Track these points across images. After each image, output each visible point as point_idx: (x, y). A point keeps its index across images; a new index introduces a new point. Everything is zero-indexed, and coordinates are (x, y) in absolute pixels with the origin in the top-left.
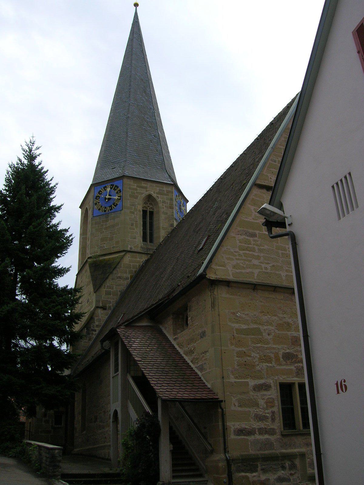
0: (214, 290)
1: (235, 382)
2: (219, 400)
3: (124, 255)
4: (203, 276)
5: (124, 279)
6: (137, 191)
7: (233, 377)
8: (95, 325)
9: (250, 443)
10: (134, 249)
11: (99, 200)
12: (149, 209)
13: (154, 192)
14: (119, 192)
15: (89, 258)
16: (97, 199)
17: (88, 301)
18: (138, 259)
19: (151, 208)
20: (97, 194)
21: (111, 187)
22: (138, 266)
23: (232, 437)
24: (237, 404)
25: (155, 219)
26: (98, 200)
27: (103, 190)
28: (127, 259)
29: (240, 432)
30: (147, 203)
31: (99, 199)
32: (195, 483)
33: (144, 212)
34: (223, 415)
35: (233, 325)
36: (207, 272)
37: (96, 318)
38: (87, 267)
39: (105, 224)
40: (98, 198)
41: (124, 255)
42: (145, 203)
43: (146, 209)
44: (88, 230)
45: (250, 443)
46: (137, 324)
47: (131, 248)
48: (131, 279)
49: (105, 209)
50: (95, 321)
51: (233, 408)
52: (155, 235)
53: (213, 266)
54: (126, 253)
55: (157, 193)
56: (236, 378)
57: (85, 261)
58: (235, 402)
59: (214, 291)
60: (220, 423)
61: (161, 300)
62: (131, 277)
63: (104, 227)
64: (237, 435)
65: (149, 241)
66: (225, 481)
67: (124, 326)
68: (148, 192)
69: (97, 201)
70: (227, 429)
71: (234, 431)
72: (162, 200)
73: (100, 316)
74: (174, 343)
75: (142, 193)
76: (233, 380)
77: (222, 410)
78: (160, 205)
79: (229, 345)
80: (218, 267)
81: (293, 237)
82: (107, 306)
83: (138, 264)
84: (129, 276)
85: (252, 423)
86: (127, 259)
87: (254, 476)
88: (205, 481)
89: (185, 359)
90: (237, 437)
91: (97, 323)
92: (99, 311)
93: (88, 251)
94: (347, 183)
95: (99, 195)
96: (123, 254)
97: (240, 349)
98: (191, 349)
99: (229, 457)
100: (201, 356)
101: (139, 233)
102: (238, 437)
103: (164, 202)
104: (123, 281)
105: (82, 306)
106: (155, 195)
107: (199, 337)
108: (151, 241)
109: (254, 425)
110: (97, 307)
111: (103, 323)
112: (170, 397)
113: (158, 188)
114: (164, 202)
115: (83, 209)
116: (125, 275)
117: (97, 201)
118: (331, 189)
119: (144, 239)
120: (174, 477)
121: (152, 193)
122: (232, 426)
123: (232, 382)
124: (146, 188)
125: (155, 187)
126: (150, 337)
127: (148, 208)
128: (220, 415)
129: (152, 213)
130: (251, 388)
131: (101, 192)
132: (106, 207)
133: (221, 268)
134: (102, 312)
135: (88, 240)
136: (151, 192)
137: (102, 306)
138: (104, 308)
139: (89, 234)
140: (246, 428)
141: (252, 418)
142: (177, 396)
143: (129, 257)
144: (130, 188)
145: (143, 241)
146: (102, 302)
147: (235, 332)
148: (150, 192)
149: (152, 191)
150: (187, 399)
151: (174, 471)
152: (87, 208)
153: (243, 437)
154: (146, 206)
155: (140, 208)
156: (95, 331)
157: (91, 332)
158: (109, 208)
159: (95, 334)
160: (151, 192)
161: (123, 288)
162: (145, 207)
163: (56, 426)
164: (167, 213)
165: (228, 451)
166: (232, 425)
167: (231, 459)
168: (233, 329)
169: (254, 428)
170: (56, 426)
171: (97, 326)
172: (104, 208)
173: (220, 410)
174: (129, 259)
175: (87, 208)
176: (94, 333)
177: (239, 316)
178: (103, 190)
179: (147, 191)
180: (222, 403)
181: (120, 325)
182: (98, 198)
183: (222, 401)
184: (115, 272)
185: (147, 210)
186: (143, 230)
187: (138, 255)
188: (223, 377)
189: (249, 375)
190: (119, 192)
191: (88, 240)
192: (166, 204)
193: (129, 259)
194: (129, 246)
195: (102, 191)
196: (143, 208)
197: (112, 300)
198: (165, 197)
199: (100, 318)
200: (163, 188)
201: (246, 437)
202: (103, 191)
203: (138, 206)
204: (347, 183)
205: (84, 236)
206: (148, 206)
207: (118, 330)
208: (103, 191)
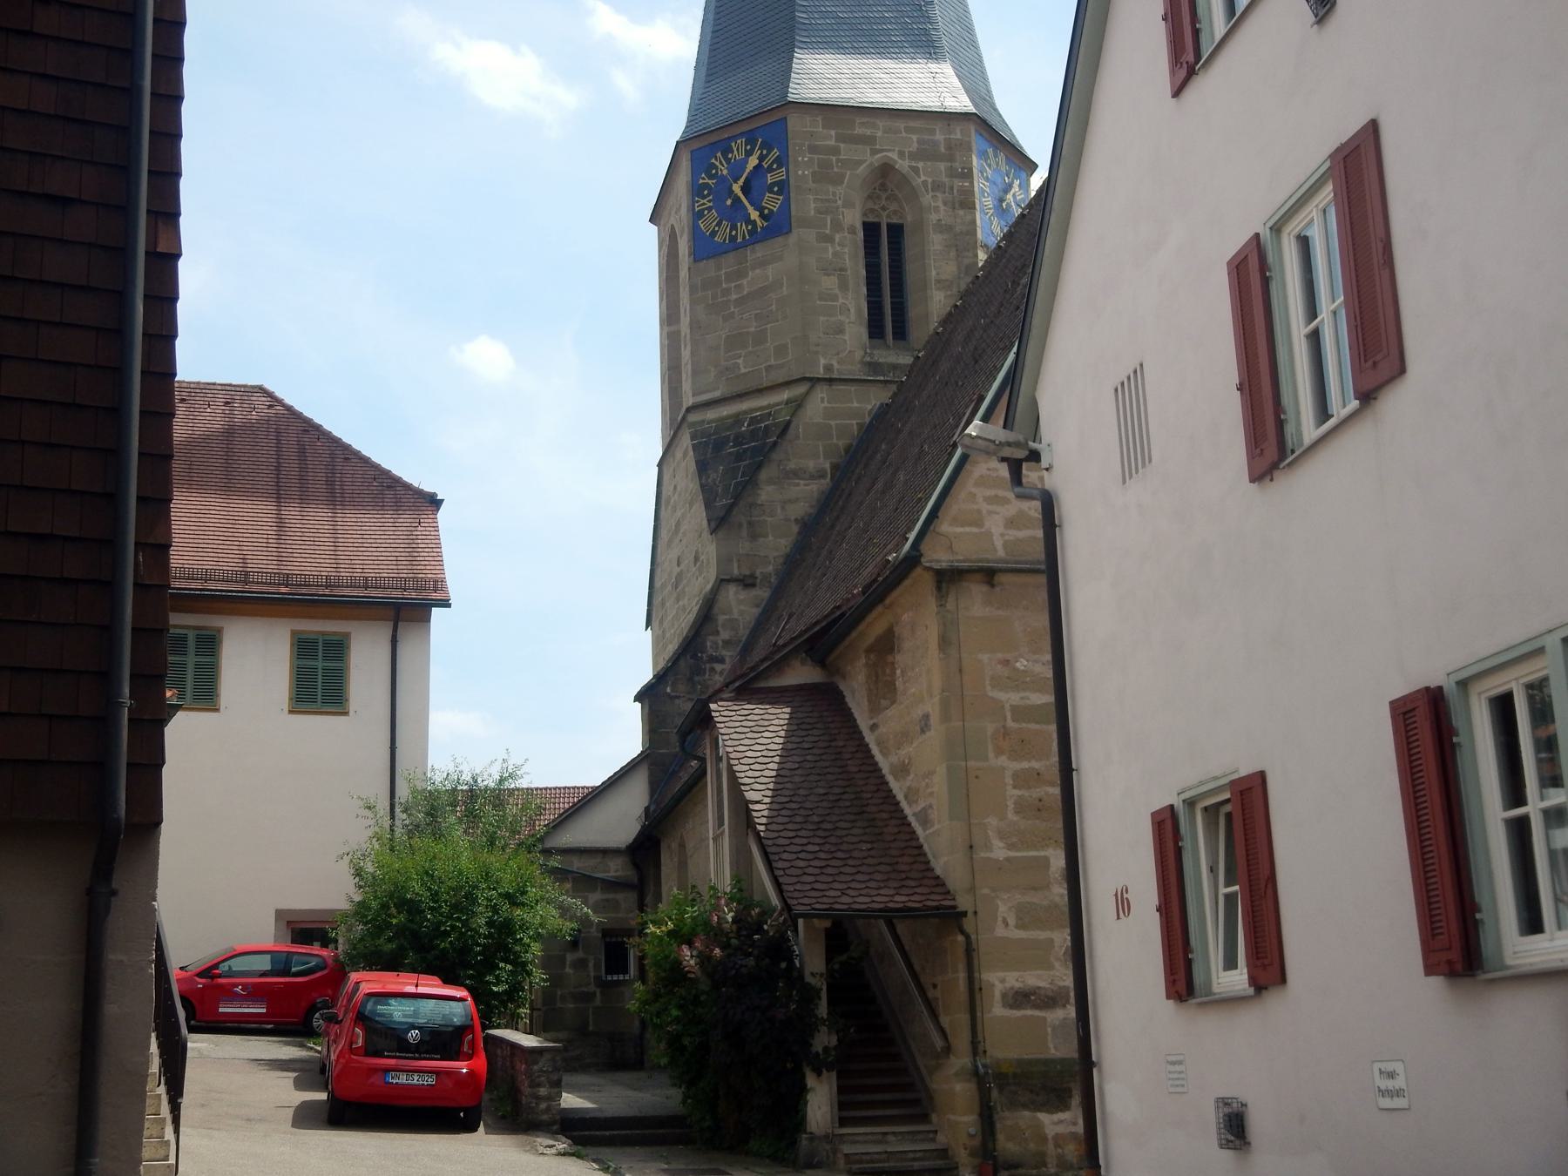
0: (947, 597)
1: (1008, 859)
2: (958, 910)
3: (808, 393)
4: (913, 560)
5: (812, 477)
6: (841, 157)
7: (1001, 845)
8: (720, 643)
9: (1049, 1030)
10: (839, 370)
11: (709, 201)
12: (888, 216)
13: (901, 154)
14: (775, 166)
15: (689, 410)
16: (704, 197)
17: (696, 559)
18: (855, 405)
19: (895, 212)
20: (703, 179)
21: (749, 147)
22: (855, 427)
23: (997, 1010)
24: (1012, 921)
25: (910, 251)
26: (705, 201)
27: (721, 162)
28: (818, 404)
29: (1021, 998)
30: (879, 197)
31: (708, 195)
32: (900, 1138)
33: (871, 230)
34: (970, 951)
35: (1001, 696)
36: (924, 548)
37: (721, 618)
38: (686, 441)
39: (735, 286)
40: (706, 192)
41: (808, 393)
42: (870, 197)
43: (876, 220)
44: (682, 311)
45: (1049, 1030)
46: (763, 684)
47: (828, 368)
48: (832, 478)
49: (731, 232)
50: (720, 629)
51: (1000, 931)
52: (913, 312)
53: (945, 526)
54: (812, 387)
55: (913, 156)
56: (1011, 847)
57: (679, 418)
58: (1005, 915)
59: (946, 601)
60: (962, 975)
61: (838, 608)
62: (835, 467)
63: (734, 297)
64: (1011, 1007)
65: (894, 333)
66: (973, 1133)
67: (731, 692)
68: (879, 155)
69: (704, 204)
70: (981, 989)
71: (1004, 996)
72: (930, 180)
73: (735, 611)
74: (870, 738)
75: (860, 163)
76: (999, 852)
77: (968, 937)
78: (926, 199)
79: (991, 755)
80: (959, 530)
81: (1048, 504)
82: (758, 574)
83: (854, 422)
84: (827, 466)
85: (1057, 974)
86: (818, 404)
87: (1061, 1122)
88: (929, 1132)
89: (891, 791)
90: (1011, 1011)
91: (725, 635)
92: (732, 594)
93: (687, 386)
94: (1136, 381)
95: (707, 181)
96: (800, 390)
97: (1025, 765)
98: (904, 761)
99: (984, 1066)
100: (924, 784)
101: (852, 310)
102: (1014, 1011)
103: (937, 187)
104: (805, 485)
105: (681, 571)
106: (903, 165)
107: (918, 728)
108: (901, 333)
109: (1065, 978)
110: (721, 582)
111: (744, 633)
112: (817, 906)
113: (915, 138)
114: (937, 187)
115: (661, 228)
116: (811, 465)
117: (704, 204)
118: (1113, 391)
119: (875, 329)
120: (843, 1122)
121: (894, 156)
122: (997, 983)
123: (997, 861)
124: (869, 140)
125: (904, 134)
126: (803, 723)
127: (884, 214)
128: (961, 952)
129: (896, 231)
130: (1057, 875)
131: (716, 168)
132: (736, 225)
133: (968, 529)
134: (744, 594)
135: (685, 346)
136: (890, 154)
137: (741, 578)
138: (747, 582)
139: (685, 321)
140: (1039, 988)
141: (1058, 959)
142: (837, 902)
143: (822, 399)
144: (813, 149)
145: (872, 336)
146: (739, 561)
147: (1009, 715)
148: (885, 153)
149: (894, 150)
150: (864, 910)
151: (842, 1106)
152: (672, 226)
153: (1029, 1012)
154: (876, 207)
155: (853, 218)
156: (721, 660)
157: (708, 666)
158: (747, 227)
159: (721, 673)
160: (890, 154)
161: (801, 509)
162: (872, 211)
163: (609, 978)
164: (950, 228)
165: (985, 1052)
166: (999, 980)
167: (990, 1071)
168: (1003, 707)
169: (1064, 987)
170: (609, 978)
171: (727, 643)
172: (728, 230)
173: (960, 938)
174: (823, 405)
175: (672, 226)
176: (718, 667)
177: (1023, 668)
178: (721, 162)
179: (874, 152)
180: (964, 919)
181: (720, 690)
182: (706, 192)
183: (964, 914)
184: (775, 456)
185: (880, 223)
186: (868, 296)
187: (853, 389)
188: (971, 847)
189: (1050, 839)
190: (775, 166)
191: (685, 346)
192: (947, 194)
193: (823, 405)
194: (822, 361)
195: (718, 164)
196: (865, 215)
197: (776, 546)
198: (942, 166)
199: (736, 616)
200: (932, 132)
201: (1037, 1013)
202: (720, 166)
203: (844, 210)
204: (1136, 381)
205: (673, 328)
206: (884, 209)
207: (713, 706)
208: (720, 166)
